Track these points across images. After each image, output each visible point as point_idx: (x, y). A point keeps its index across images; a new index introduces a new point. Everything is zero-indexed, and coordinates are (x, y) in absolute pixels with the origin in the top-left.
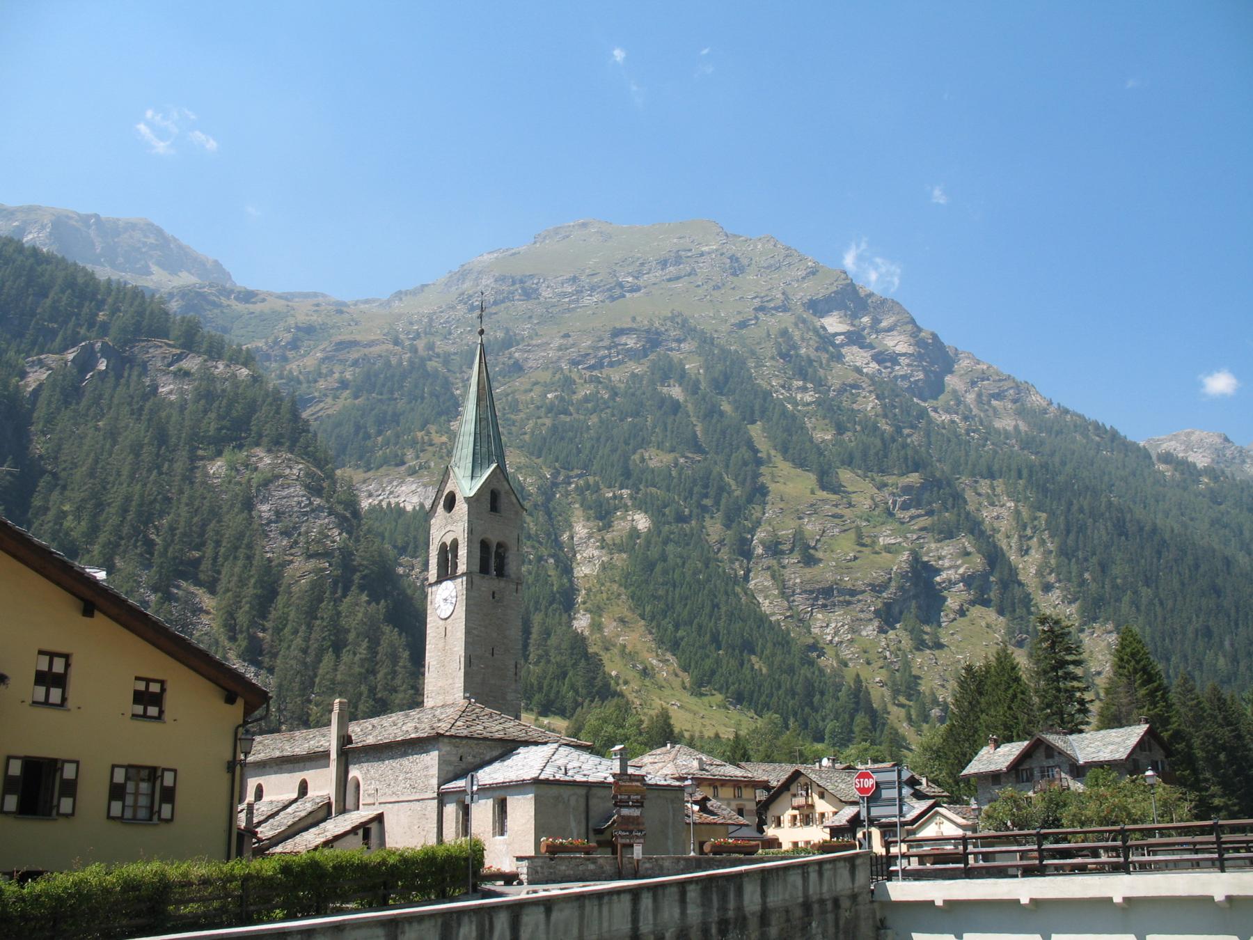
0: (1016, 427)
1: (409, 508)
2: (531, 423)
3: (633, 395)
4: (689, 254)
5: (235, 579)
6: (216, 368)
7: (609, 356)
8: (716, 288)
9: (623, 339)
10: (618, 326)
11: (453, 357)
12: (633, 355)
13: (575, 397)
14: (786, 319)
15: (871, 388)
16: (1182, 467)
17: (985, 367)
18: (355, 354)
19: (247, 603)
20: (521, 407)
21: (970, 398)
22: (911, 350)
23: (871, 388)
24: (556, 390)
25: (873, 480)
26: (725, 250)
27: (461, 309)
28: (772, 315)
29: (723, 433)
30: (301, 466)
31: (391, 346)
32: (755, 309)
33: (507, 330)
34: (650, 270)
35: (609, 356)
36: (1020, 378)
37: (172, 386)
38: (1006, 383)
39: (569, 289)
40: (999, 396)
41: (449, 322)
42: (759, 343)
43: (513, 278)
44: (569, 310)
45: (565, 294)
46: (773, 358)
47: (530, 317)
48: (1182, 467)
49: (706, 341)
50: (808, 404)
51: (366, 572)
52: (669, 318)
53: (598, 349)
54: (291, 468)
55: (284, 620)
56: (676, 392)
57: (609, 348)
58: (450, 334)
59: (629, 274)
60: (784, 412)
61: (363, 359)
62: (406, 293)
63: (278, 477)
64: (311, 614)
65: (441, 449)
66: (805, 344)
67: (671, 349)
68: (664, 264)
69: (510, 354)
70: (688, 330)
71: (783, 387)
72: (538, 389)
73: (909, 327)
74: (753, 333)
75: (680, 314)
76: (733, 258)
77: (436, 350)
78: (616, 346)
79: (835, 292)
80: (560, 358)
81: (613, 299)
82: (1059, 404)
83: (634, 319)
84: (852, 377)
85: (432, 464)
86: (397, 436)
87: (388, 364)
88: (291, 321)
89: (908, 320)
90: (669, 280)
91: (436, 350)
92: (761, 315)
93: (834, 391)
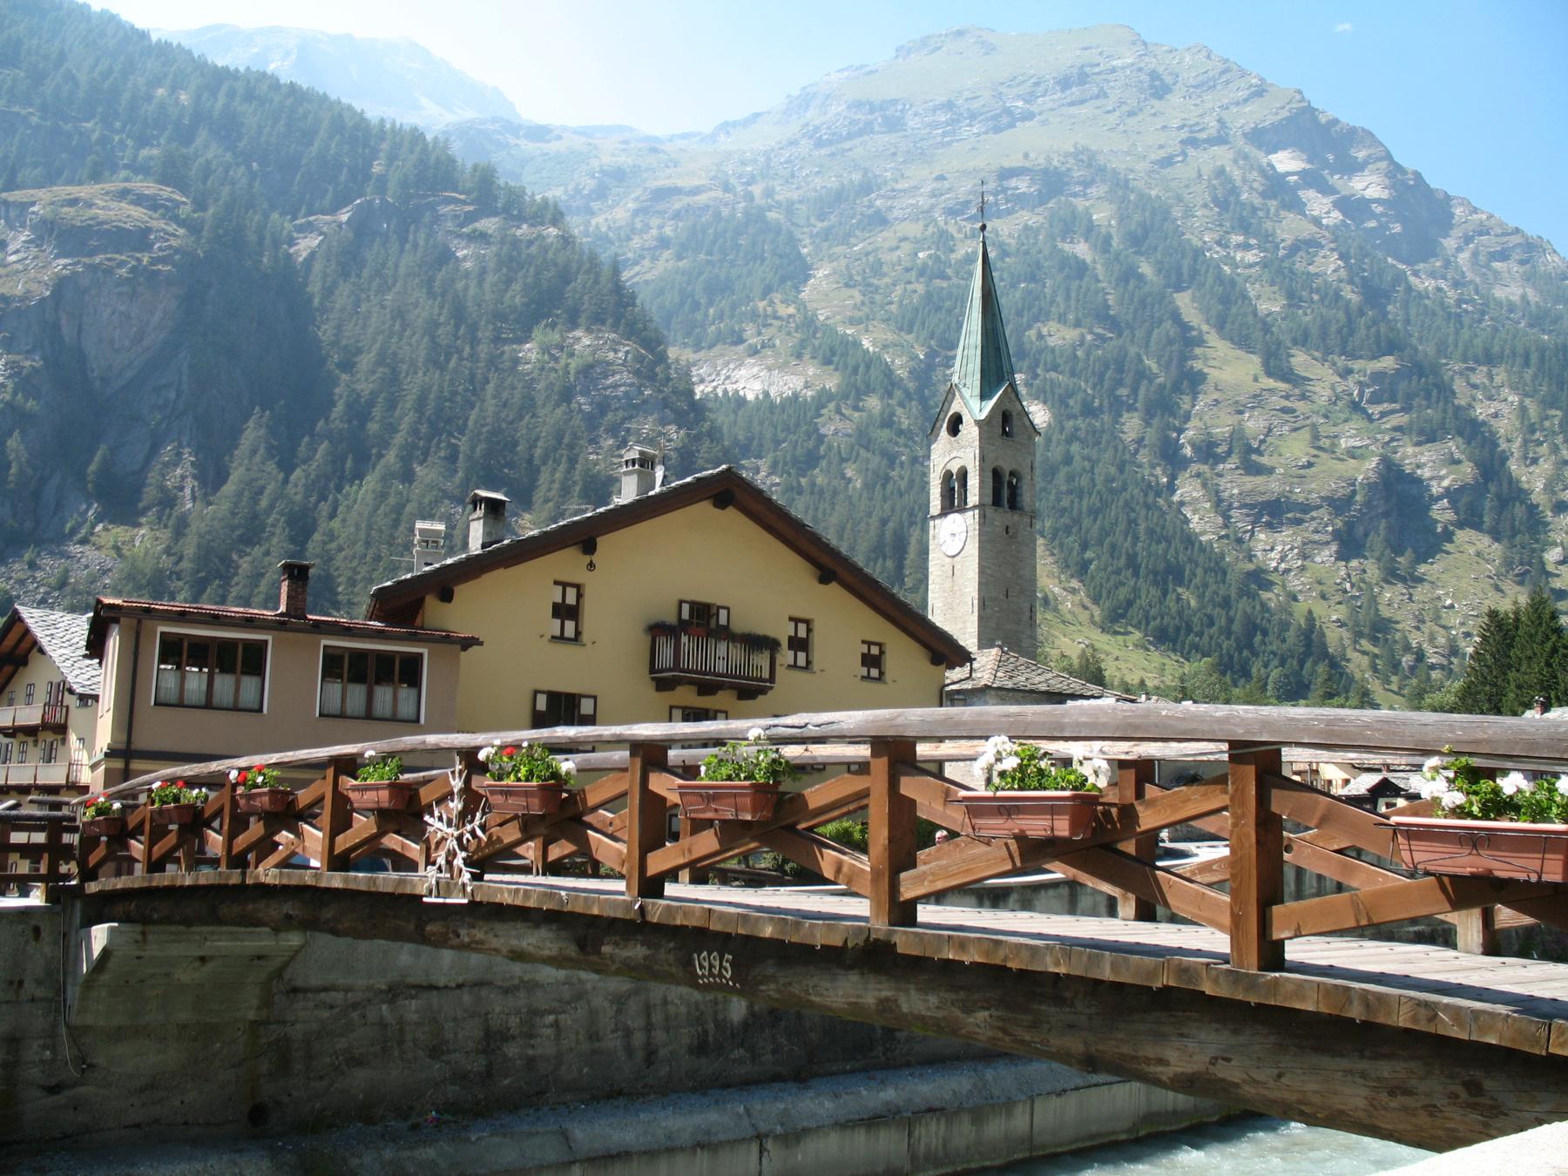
1: (750, 397)
2: (899, 290)
3: (1027, 253)
4: (1097, 70)
5: (556, 486)
6: (519, 227)
8: (1131, 114)
9: (1013, 182)
10: (1006, 164)
11: (797, 206)
12: (1021, 200)
13: (953, 256)
15: (1332, 245)
18: (677, 204)
20: (885, 269)
22: (1385, 195)
23: (1332, 245)
24: (929, 248)
25: (1334, 364)
26: (1143, 65)
27: (805, 146)
28: (1205, 149)
31: (719, 194)
32: (1182, 142)
34: (1046, 91)
36: (1532, 231)
37: (465, 252)
39: (943, 117)
40: (1503, 256)
42: (1187, 187)
43: (871, 104)
44: (943, 145)
46: (1205, 206)
47: (894, 154)
49: (1120, 186)
50: (1251, 266)
52: (1071, 154)
54: (616, 351)
57: (996, 194)
58: (793, 176)
59: (1019, 97)
60: (1220, 277)
61: (687, 211)
62: (735, 124)
63: (599, 362)
68: (1064, 83)
70: (1095, 170)
71: (1219, 243)
72: (906, 246)
73: (1383, 165)
75: (1086, 149)
76: (1154, 75)
78: (1004, 190)
80: (933, 206)
81: (997, 130)
83: (1026, 156)
85: (778, 342)
86: (734, 307)
88: (595, 163)
90: (1072, 104)
91: (777, 198)
92: (1191, 152)
93: (1284, 248)
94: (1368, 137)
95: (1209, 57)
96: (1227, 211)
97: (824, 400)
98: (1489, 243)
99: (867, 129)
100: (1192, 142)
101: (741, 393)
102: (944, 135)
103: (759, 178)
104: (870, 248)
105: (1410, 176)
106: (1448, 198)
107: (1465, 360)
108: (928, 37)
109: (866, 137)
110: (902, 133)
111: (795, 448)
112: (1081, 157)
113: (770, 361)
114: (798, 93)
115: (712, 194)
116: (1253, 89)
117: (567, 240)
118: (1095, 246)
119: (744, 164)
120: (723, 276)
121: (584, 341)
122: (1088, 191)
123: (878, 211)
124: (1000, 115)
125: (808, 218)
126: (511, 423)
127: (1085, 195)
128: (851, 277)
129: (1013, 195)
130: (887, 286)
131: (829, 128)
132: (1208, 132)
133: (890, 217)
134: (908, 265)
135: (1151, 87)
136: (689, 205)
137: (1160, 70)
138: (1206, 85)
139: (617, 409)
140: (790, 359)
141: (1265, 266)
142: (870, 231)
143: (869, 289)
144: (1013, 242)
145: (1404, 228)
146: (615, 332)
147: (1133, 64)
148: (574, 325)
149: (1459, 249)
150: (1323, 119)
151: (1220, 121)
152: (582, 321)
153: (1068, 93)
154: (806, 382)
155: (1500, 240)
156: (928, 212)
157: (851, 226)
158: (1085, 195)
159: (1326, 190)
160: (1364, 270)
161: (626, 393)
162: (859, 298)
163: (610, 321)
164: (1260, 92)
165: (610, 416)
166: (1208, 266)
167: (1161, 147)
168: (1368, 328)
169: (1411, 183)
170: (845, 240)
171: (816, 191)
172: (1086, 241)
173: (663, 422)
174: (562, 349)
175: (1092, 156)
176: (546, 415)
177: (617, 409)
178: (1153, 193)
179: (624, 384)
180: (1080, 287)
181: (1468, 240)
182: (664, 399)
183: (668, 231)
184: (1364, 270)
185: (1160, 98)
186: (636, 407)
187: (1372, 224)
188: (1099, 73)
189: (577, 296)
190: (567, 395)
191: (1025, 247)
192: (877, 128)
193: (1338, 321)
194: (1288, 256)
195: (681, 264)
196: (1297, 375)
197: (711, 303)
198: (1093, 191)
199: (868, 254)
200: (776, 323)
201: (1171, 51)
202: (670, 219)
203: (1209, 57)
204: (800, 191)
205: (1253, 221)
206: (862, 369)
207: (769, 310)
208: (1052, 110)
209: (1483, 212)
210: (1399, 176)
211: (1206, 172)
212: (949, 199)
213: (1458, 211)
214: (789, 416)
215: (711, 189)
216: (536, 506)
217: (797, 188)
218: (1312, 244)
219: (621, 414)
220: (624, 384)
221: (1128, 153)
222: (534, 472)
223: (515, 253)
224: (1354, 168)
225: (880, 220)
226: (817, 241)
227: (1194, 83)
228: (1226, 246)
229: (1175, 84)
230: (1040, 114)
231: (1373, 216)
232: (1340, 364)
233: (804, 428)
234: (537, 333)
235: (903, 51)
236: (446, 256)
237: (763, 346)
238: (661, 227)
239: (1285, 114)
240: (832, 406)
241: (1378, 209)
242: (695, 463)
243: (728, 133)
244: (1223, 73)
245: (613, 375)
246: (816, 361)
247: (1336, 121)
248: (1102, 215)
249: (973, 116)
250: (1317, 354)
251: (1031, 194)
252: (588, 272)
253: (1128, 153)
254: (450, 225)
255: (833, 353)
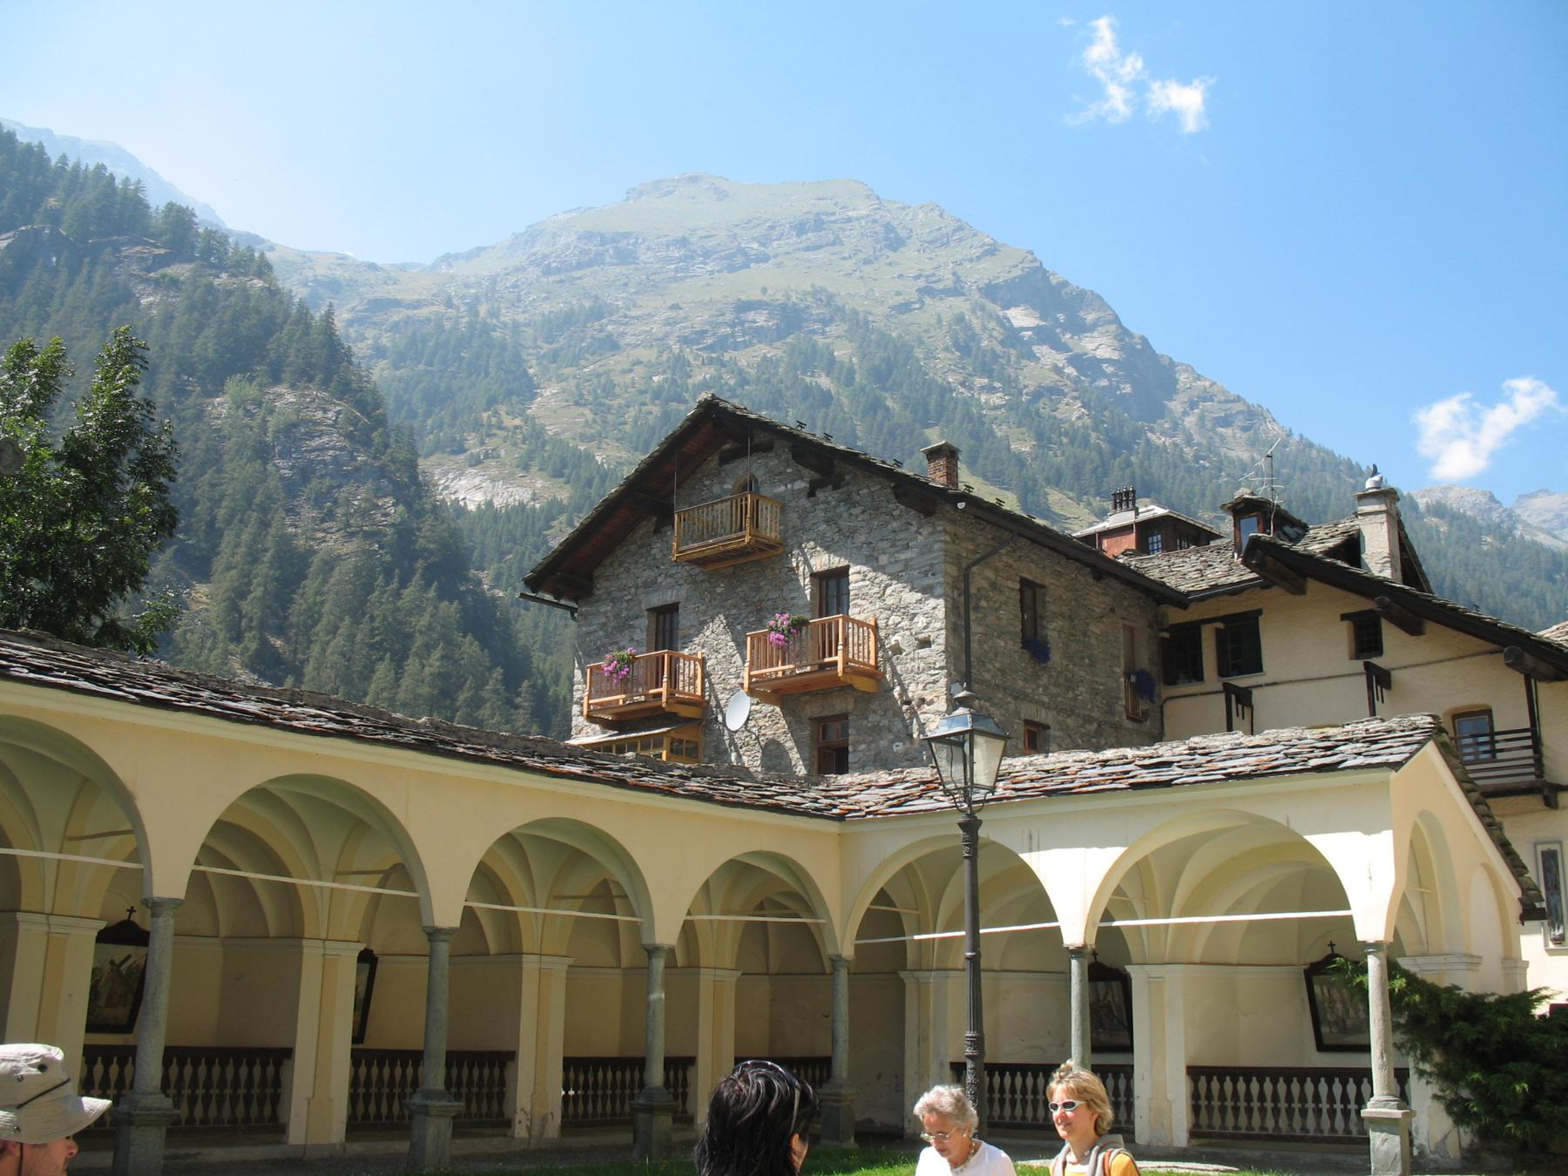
0: (1253, 460)
1: (472, 507)
2: (632, 412)
3: (768, 381)
4: (832, 218)
5: (242, 550)
6: (217, 277)
7: (733, 335)
8: (867, 262)
9: (751, 316)
10: (744, 298)
11: (523, 328)
12: (759, 334)
13: (690, 381)
14: (960, 305)
15: (1075, 394)
16: (1459, 522)
17: (1207, 384)
18: (396, 316)
19: (259, 585)
20: (617, 390)
21: (1190, 421)
22: (1115, 356)
23: (1075, 394)
24: (665, 372)
25: (1089, 504)
26: (877, 217)
27: (533, 273)
28: (941, 299)
29: (892, 434)
30: (338, 408)
31: (442, 308)
32: (919, 290)
33: (596, 298)
34: (782, 235)
35: (733, 335)
36: (1252, 400)
37: (151, 299)
38: (1233, 405)
39: (676, 253)
40: (1226, 421)
41: (517, 287)
42: (927, 331)
43: (602, 236)
44: (675, 279)
45: (667, 260)
46: (946, 349)
47: (626, 285)
48: (1459, 522)
49: (859, 326)
50: (996, 408)
51: (433, 559)
52: (809, 293)
53: (719, 325)
54: (325, 411)
55: (313, 616)
56: (824, 382)
57: (733, 325)
58: (519, 300)
59: (754, 239)
60: (968, 416)
61: (406, 323)
62: (457, 257)
63: (305, 422)
64: (357, 610)
65: (515, 433)
66: (986, 335)
67: (814, 332)
68: (800, 228)
69: (601, 325)
70: (834, 311)
71: (963, 384)
72: (639, 370)
73: (1113, 327)
74: (921, 319)
75: (822, 290)
76: (889, 228)
77: (502, 319)
78: (742, 323)
79: (1018, 277)
80: (666, 335)
81: (732, 269)
82: (1301, 436)
83: (764, 290)
84: (1050, 378)
85: (502, 453)
86: (455, 416)
87: (440, 327)
88: (309, 273)
89: (1112, 317)
90: (807, 249)
91: (502, 319)
92: (928, 300)
93: (1027, 394)
94: (1097, 301)
95: (941, 216)
96: (969, 356)
97: (554, 512)
98: (1213, 409)
99: (596, 260)
100: (928, 291)
101: (462, 503)
102: (677, 270)
103: (483, 300)
104: (601, 370)
105: (1137, 340)
106: (1172, 364)
107: (1214, 510)
108: (661, 181)
109: (596, 268)
110: (633, 266)
111: (522, 560)
112: (819, 296)
113: (494, 472)
114: (523, 231)
115: (434, 308)
116: (986, 248)
117: (273, 292)
118: (839, 380)
119: (467, 286)
120: (443, 386)
121: (286, 398)
122: (827, 329)
123: (610, 336)
124: (734, 255)
125: (535, 341)
126: (191, 480)
127: (823, 333)
128: (581, 396)
129: (750, 328)
130: (620, 406)
131: (557, 257)
132: (944, 283)
133: (622, 343)
134: (643, 388)
135: (886, 239)
136: (408, 317)
137: (895, 224)
138: (940, 241)
139: (322, 476)
140: (517, 470)
141: (1011, 408)
142: (601, 355)
143: (601, 409)
144: (753, 372)
145: (1132, 387)
146: (326, 391)
147: (868, 216)
148: (277, 380)
149: (1185, 413)
150: (1054, 281)
151: (954, 274)
152: (286, 376)
153: (804, 237)
154: (534, 494)
155: (1224, 406)
156: (662, 339)
157: (582, 348)
158: (823, 333)
159: (1059, 347)
160: (1104, 422)
161: (335, 458)
162: (590, 416)
163: (319, 377)
164: (992, 251)
165: (314, 483)
166: (956, 403)
167: (898, 294)
168: (1122, 469)
169: (1139, 347)
170: (575, 361)
171: (543, 315)
172: (828, 375)
173: (379, 493)
174: (260, 405)
175: (831, 297)
176: (234, 470)
177: (322, 476)
178: (894, 335)
179: (333, 448)
180: (827, 414)
181: (1193, 405)
182: (379, 467)
183: (385, 341)
184: (1104, 422)
185: (895, 250)
186: (347, 475)
187: (1104, 383)
188: (834, 222)
189: (281, 350)
190: (262, 453)
191: (766, 376)
192: (608, 260)
193: (1092, 461)
194: (1029, 402)
195: (398, 373)
196: (1054, 513)
197: (428, 414)
198: (832, 330)
199: (599, 376)
200: (503, 433)
201: (904, 208)
202: (387, 331)
203: (941, 216)
204: (527, 315)
205: (995, 367)
206: (596, 481)
207: (494, 420)
208: (787, 253)
209: (1206, 379)
210: (1127, 339)
211: (946, 318)
212: (685, 328)
213: (1182, 377)
214: (516, 526)
215: (433, 304)
216: (215, 577)
217: (524, 312)
218: (1054, 391)
219: (327, 481)
220: (333, 448)
221: (866, 297)
222: (214, 533)
223: (210, 298)
224: (1081, 329)
225: (612, 345)
226: (545, 362)
227: (929, 238)
228: (970, 388)
229: (908, 238)
230: (775, 256)
231: (1105, 375)
232: (1095, 504)
233: (531, 540)
234: (231, 385)
235: (635, 193)
236: (128, 297)
237: (487, 456)
238: (376, 338)
239: (1017, 272)
240: (563, 518)
241: (1109, 369)
242: (415, 542)
243: (450, 265)
244: (955, 231)
245: (320, 437)
246: (544, 474)
247: (1066, 284)
248: (843, 352)
249: (707, 255)
250: (1071, 494)
251: (769, 328)
252: (297, 322)
253: (866, 297)
254: (135, 268)
255: (564, 466)
